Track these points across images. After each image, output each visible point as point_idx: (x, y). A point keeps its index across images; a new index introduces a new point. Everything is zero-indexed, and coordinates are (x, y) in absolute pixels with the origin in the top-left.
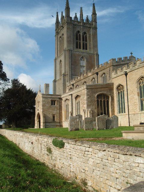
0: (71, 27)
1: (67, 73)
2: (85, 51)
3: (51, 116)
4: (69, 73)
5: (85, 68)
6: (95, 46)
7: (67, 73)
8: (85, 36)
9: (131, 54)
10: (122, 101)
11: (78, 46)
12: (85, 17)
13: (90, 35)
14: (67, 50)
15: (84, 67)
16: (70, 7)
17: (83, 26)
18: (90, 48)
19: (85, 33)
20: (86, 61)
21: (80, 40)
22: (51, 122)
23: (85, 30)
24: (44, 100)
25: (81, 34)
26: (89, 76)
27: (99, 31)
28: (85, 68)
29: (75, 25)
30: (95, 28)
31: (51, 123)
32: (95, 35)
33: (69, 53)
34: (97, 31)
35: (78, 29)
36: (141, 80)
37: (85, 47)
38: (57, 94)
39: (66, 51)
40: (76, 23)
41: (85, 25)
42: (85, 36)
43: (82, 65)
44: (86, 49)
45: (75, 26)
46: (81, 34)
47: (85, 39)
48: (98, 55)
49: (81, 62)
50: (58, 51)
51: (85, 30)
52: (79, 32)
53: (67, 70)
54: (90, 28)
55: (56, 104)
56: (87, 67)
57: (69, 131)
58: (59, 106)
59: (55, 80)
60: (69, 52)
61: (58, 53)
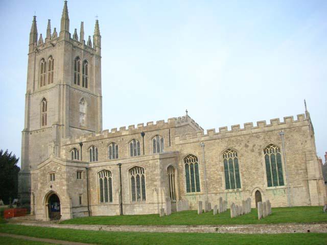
0: (70, 48)
1: (63, 122)
2: (84, 89)
3: (76, 197)
4: (66, 122)
5: (85, 116)
6: (99, 84)
7: (63, 122)
8: (85, 65)
9: (187, 112)
10: (192, 177)
11: (76, 80)
12: (86, 39)
13: (92, 65)
14: (64, 85)
15: (84, 114)
16: (69, 18)
17: (84, 50)
18: (92, 87)
19: (85, 61)
20: (88, 106)
21: (79, 71)
22: (78, 207)
23: (87, 57)
24: (68, 170)
25: (81, 62)
26: (123, 136)
27: (102, 59)
28: (85, 116)
29: (75, 47)
30: (99, 57)
31: (78, 209)
32: (99, 67)
33: (67, 91)
34: (100, 61)
35: (78, 54)
36: (227, 152)
37: (85, 84)
38: (83, 160)
39: (62, 86)
40: (75, 43)
41: (86, 50)
42: (85, 65)
43: (81, 111)
44: (86, 87)
45: (74, 49)
46: (81, 62)
47: (85, 71)
48: (101, 97)
49: (81, 106)
50: (34, 81)
51: (87, 57)
52: (78, 58)
53: (63, 117)
54: (92, 54)
55: (82, 177)
56: (87, 115)
57: (214, 214)
58: (86, 180)
59: (27, 129)
60: (67, 88)
61: (34, 83)
